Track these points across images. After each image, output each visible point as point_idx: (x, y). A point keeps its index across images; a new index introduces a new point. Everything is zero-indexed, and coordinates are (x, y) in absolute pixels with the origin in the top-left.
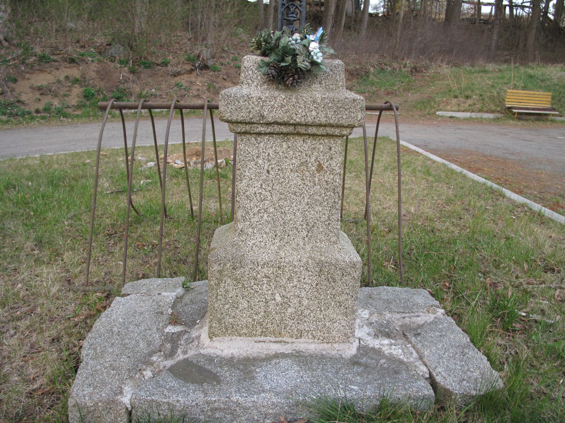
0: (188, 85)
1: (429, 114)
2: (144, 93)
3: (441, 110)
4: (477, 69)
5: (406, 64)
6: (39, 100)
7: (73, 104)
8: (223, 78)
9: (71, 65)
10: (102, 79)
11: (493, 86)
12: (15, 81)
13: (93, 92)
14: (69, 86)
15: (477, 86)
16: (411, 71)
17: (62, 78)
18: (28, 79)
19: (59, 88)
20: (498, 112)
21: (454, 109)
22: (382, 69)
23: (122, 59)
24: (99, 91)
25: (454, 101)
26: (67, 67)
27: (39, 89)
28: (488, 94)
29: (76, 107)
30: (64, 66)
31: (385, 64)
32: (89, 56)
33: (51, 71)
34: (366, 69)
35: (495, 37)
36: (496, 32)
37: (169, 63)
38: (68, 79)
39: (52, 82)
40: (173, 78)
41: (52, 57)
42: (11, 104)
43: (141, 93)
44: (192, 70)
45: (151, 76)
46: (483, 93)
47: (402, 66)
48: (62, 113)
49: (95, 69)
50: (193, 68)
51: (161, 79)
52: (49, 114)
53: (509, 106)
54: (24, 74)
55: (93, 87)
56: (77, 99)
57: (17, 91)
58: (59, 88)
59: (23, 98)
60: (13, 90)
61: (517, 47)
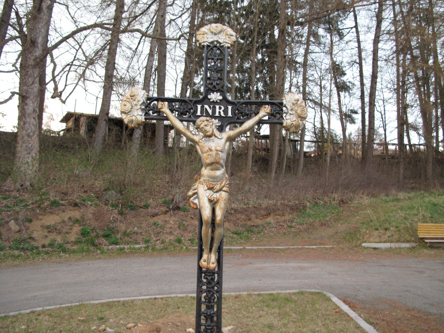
0: (163, 224)
1: (356, 246)
2: (128, 231)
3: (365, 242)
4: (391, 198)
5: (334, 198)
6: (47, 237)
7: (72, 240)
8: (191, 217)
9: (75, 208)
10: (97, 220)
11: (405, 218)
12: (30, 221)
13: (88, 230)
14: (71, 225)
15: (393, 219)
16: (339, 203)
17: (66, 219)
18: (41, 219)
19: (63, 227)
20: (413, 241)
21: (376, 240)
22: (316, 203)
23: (114, 202)
24: (93, 230)
25: (376, 233)
26: (71, 210)
27: (48, 227)
28: (402, 225)
29: (74, 243)
30: (69, 209)
31: (318, 199)
32: (89, 201)
33: (59, 213)
34: (303, 203)
35: (402, 171)
36: (402, 168)
37: (149, 206)
38: (71, 219)
39: (58, 222)
40: (152, 218)
41: (61, 202)
42: (24, 240)
43: (126, 231)
44: (167, 211)
45: (135, 217)
46: (398, 225)
47: (332, 200)
48: (62, 249)
49: (92, 212)
50: (168, 210)
51: (142, 219)
52: (53, 248)
53: (421, 236)
54: (38, 215)
55: (89, 226)
56: (76, 236)
57: (31, 229)
58: (63, 227)
59: (35, 235)
60: (28, 229)
61: (420, 177)
